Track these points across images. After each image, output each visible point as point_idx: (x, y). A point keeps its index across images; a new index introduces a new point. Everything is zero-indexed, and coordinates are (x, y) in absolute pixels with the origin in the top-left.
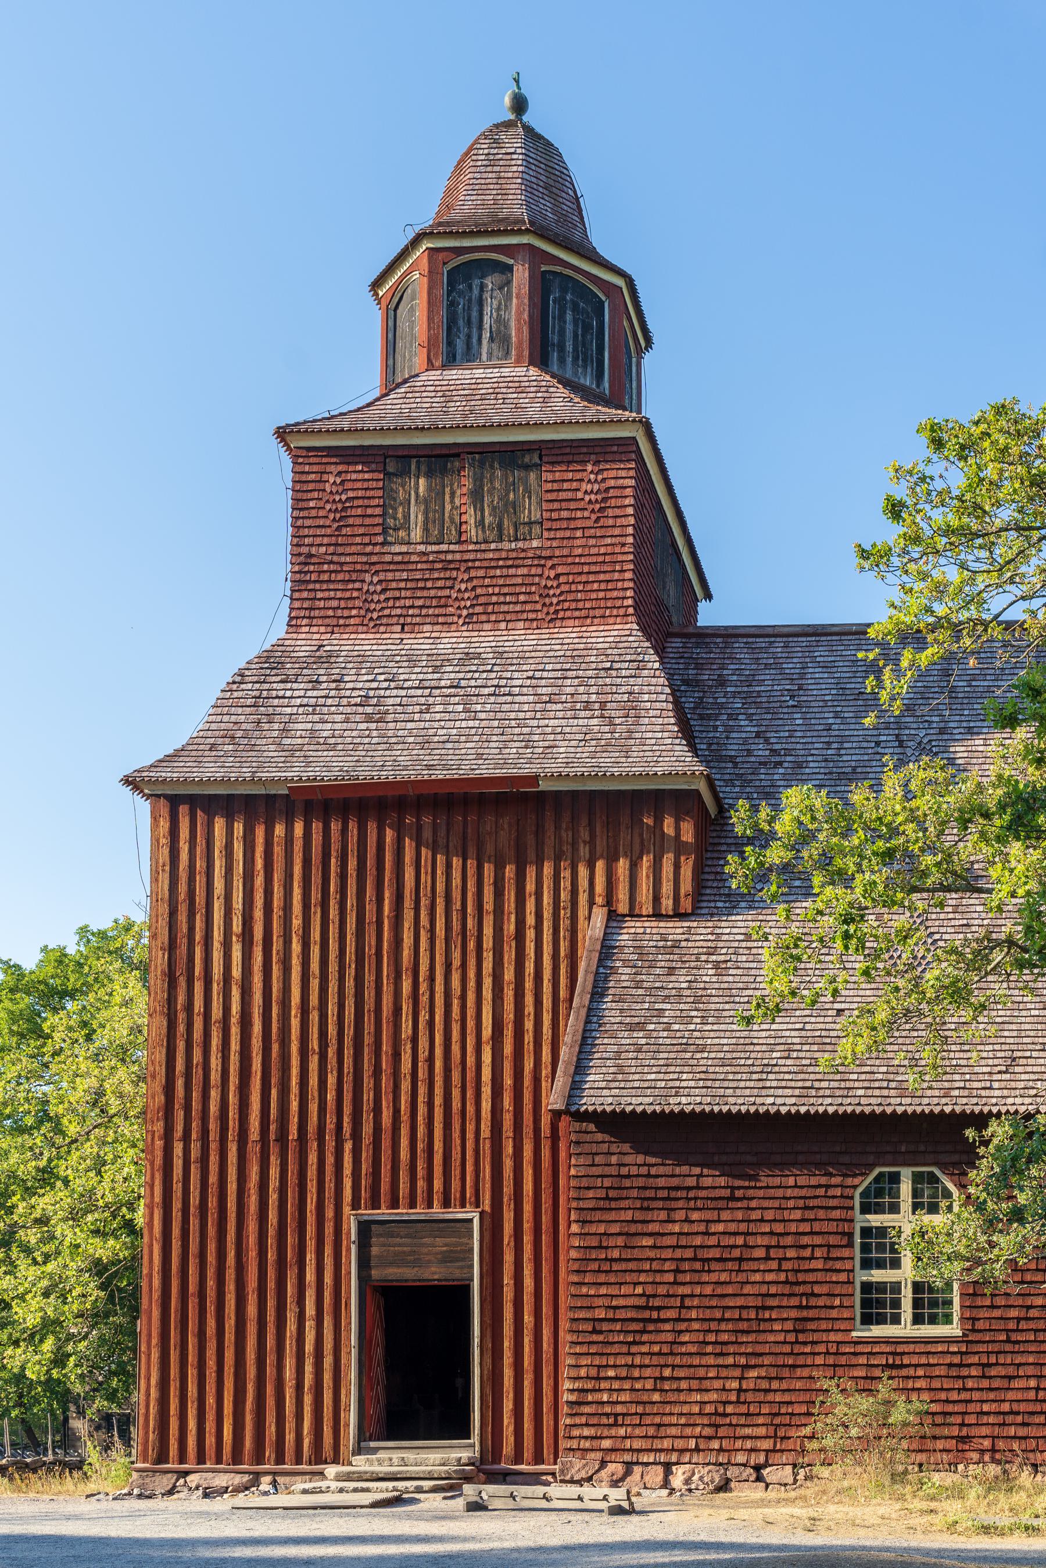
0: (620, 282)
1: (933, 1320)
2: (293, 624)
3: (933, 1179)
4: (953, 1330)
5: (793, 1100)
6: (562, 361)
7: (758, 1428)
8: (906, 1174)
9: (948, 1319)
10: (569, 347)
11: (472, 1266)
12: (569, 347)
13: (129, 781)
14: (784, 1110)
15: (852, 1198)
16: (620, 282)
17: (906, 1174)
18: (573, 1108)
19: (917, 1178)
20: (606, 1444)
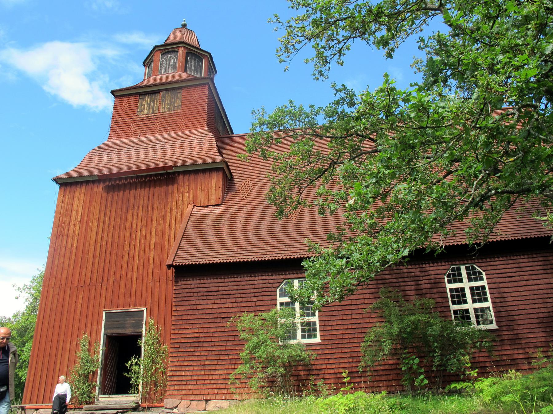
0: (207, 55)
1: (310, 337)
2: (110, 138)
3: (474, 268)
4: (318, 340)
5: (253, 257)
6: (191, 71)
7: (223, 389)
8: (463, 268)
9: (315, 336)
10: (193, 68)
11: (143, 321)
12: (193, 68)
13: (54, 180)
14: (249, 260)
15: (276, 291)
16: (207, 55)
17: (463, 268)
18: (174, 264)
19: (467, 269)
20: (184, 392)
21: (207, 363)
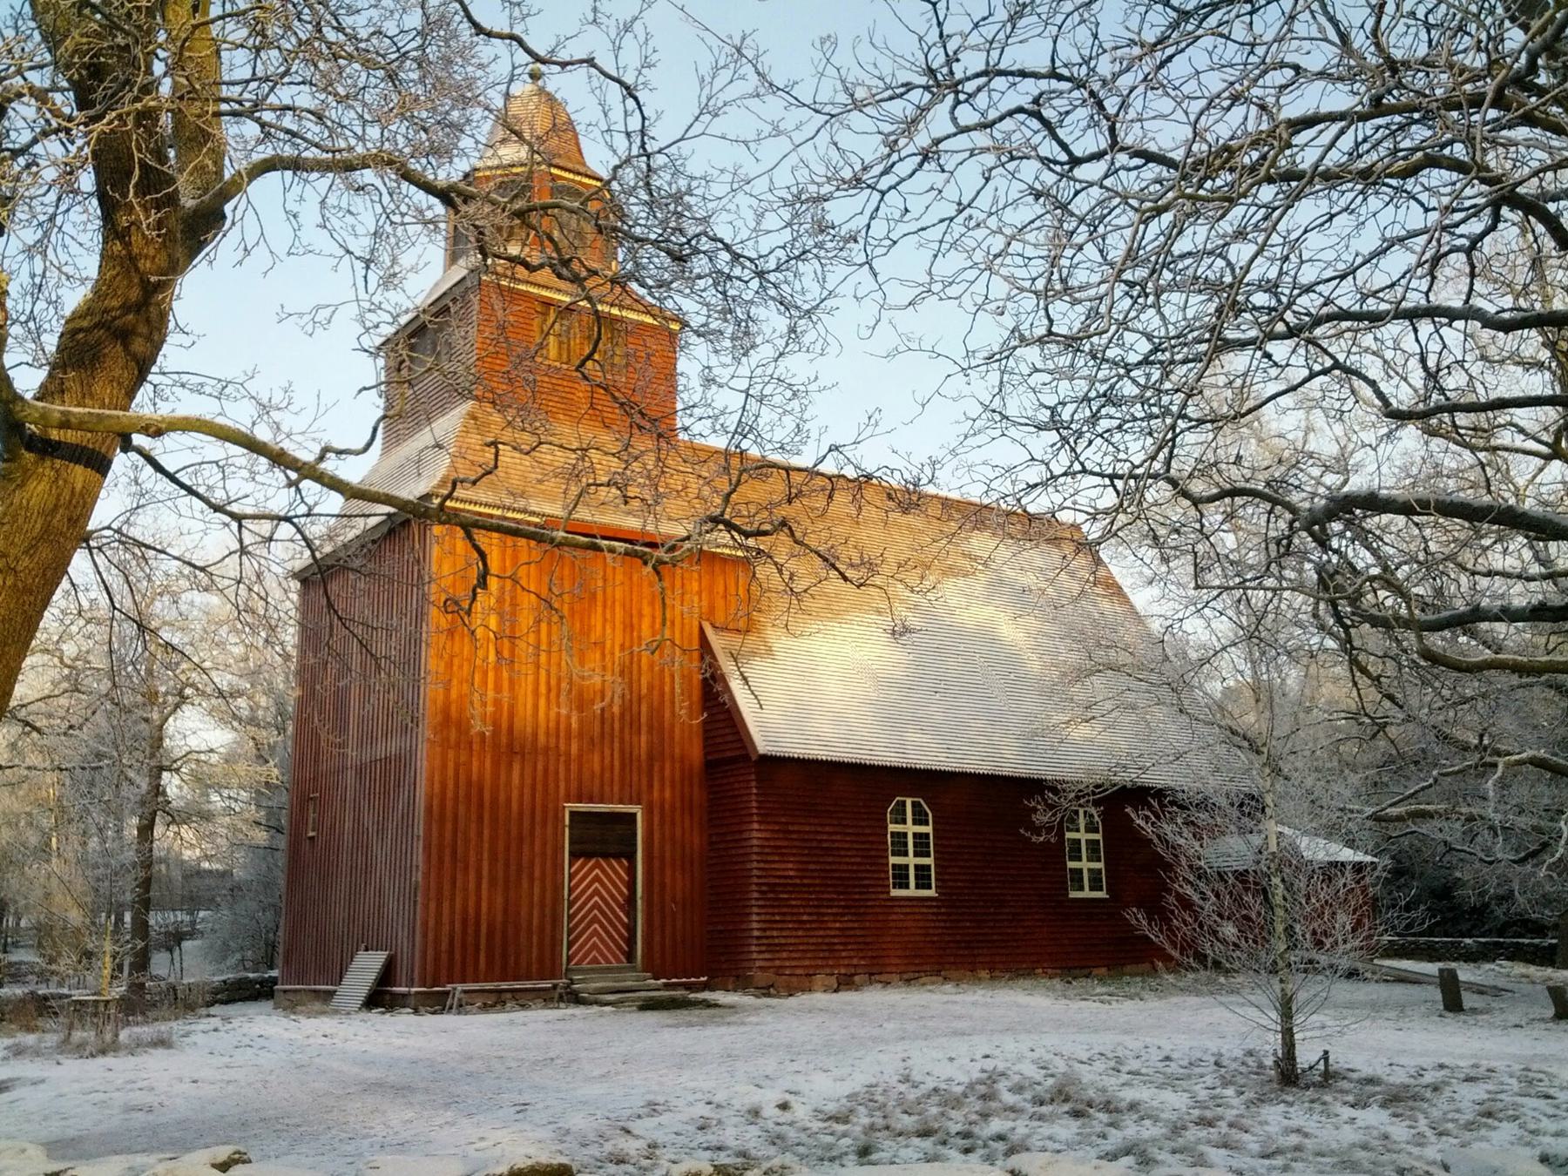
8: (909, 801)
21: (805, 918)
